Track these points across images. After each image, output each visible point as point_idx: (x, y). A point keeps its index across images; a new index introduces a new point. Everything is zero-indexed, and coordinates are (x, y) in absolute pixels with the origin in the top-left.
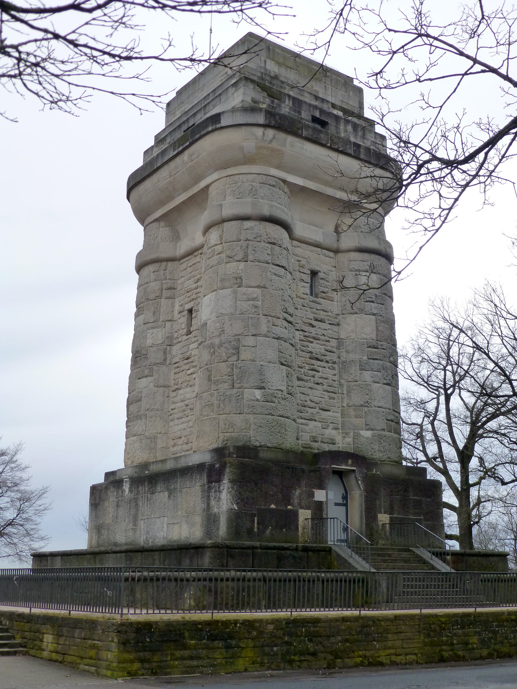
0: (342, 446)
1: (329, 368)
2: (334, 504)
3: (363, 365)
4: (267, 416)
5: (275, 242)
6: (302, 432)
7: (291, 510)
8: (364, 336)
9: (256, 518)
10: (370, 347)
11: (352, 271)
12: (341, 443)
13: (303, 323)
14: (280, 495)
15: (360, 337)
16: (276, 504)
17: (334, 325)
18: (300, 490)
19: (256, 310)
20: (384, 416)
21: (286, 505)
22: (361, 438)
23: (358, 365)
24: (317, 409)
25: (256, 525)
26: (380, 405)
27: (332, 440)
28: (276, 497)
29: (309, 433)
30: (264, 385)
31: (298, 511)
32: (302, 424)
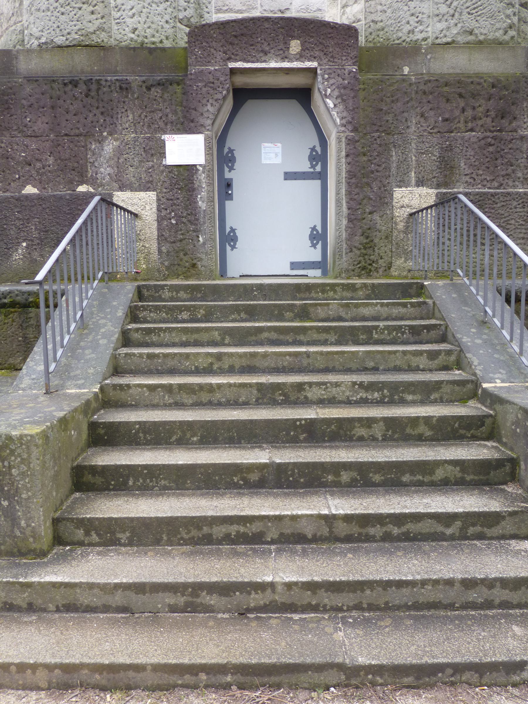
14: (51, 160)
16: (39, 184)
18: (116, 140)
21: (72, 184)
28: (38, 165)
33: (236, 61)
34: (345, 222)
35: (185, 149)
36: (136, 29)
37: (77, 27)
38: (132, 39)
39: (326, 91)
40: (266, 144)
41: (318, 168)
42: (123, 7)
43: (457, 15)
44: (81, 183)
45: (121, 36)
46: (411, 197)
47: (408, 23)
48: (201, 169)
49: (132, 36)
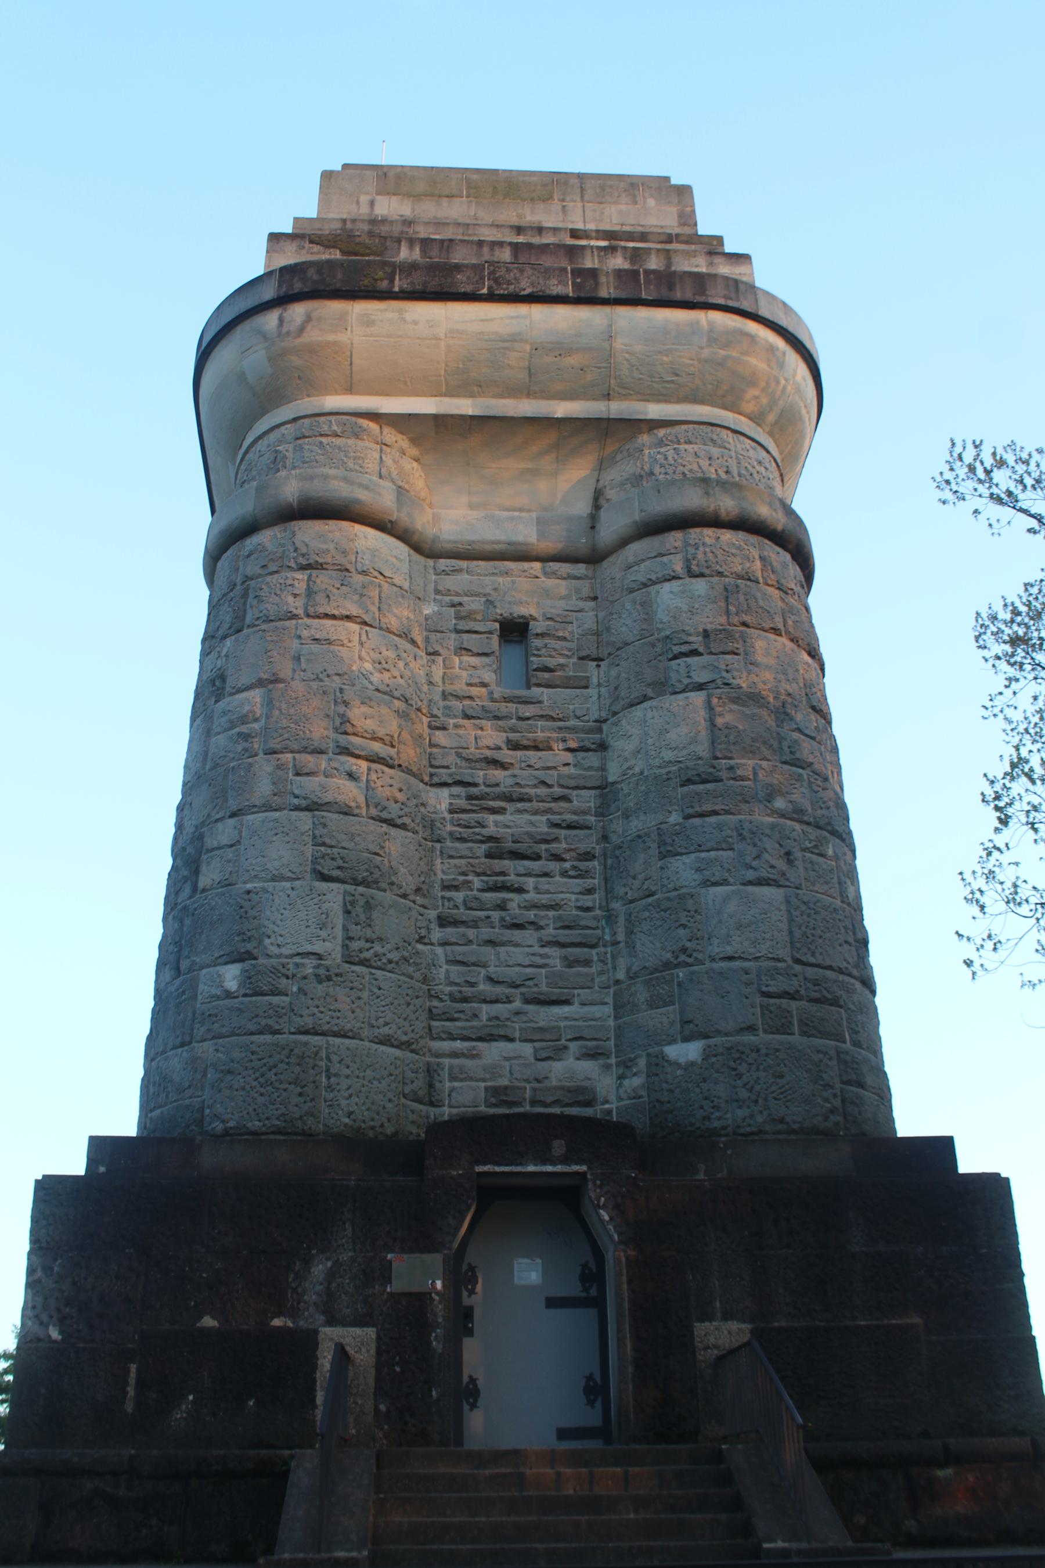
0: (617, 1108)
1: (564, 874)
2: (543, 1303)
3: (669, 841)
4: (254, 1038)
5: (321, 560)
6: (453, 1078)
7: (283, 1329)
8: (668, 755)
9: (133, 1368)
10: (689, 781)
11: (631, 591)
12: (612, 1097)
13: (464, 764)
15: (657, 762)
17: (588, 750)
19: (247, 745)
20: (747, 984)
22: (669, 1070)
23: (654, 845)
24: (517, 1004)
25: (131, 1391)
26: (729, 950)
27: (582, 1090)
29: (484, 1080)
30: (250, 946)
31: (316, 1332)
32: (454, 1055)
33: (485, 1164)
34: (630, 1369)
35: (419, 1273)
36: (352, 1113)
37: (279, 1112)
38: (346, 1125)
39: (599, 1200)
40: (521, 1260)
41: (593, 1292)
42: (338, 1088)
43: (760, 1101)
44: (278, 1315)
45: (332, 1121)
46: (720, 1334)
47: (702, 1107)
48: (437, 1298)
49: (347, 1120)
